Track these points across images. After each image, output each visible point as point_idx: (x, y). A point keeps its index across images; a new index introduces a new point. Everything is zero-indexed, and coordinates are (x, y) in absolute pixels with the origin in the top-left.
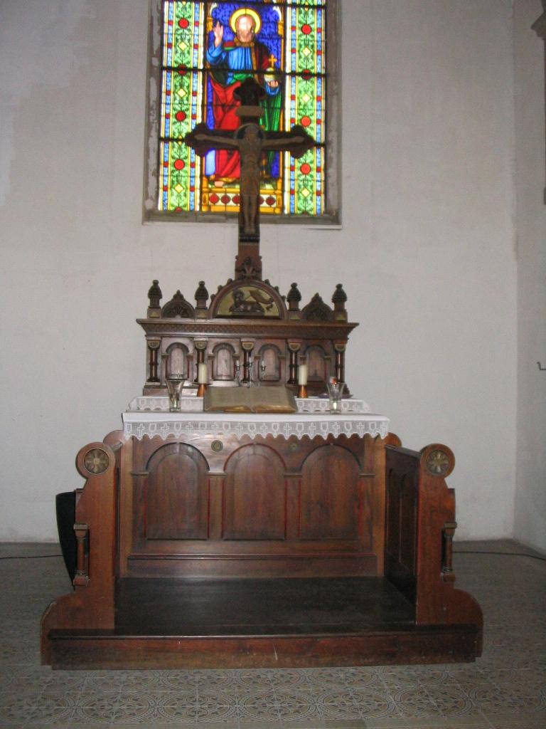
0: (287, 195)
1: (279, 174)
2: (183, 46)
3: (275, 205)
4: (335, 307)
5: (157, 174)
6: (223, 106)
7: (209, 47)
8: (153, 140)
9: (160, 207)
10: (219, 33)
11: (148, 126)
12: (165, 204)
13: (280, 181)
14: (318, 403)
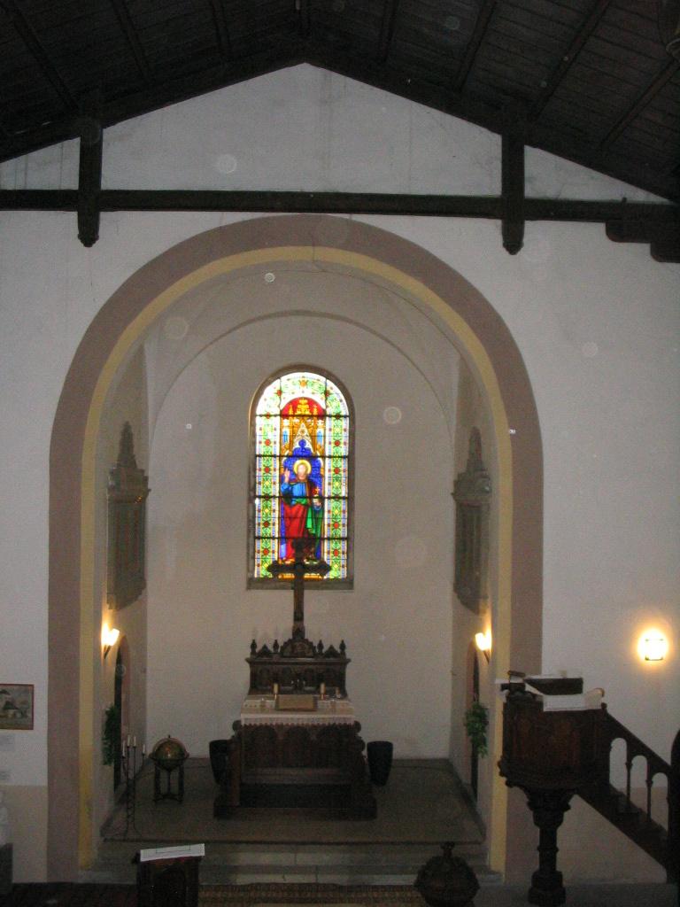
2: (267, 483)
5: (254, 558)
6: (290, 518)
8: (252, 539)
9: (256, 576)
10: (287, 474)
11: (249, 531)
12: (258, 574)
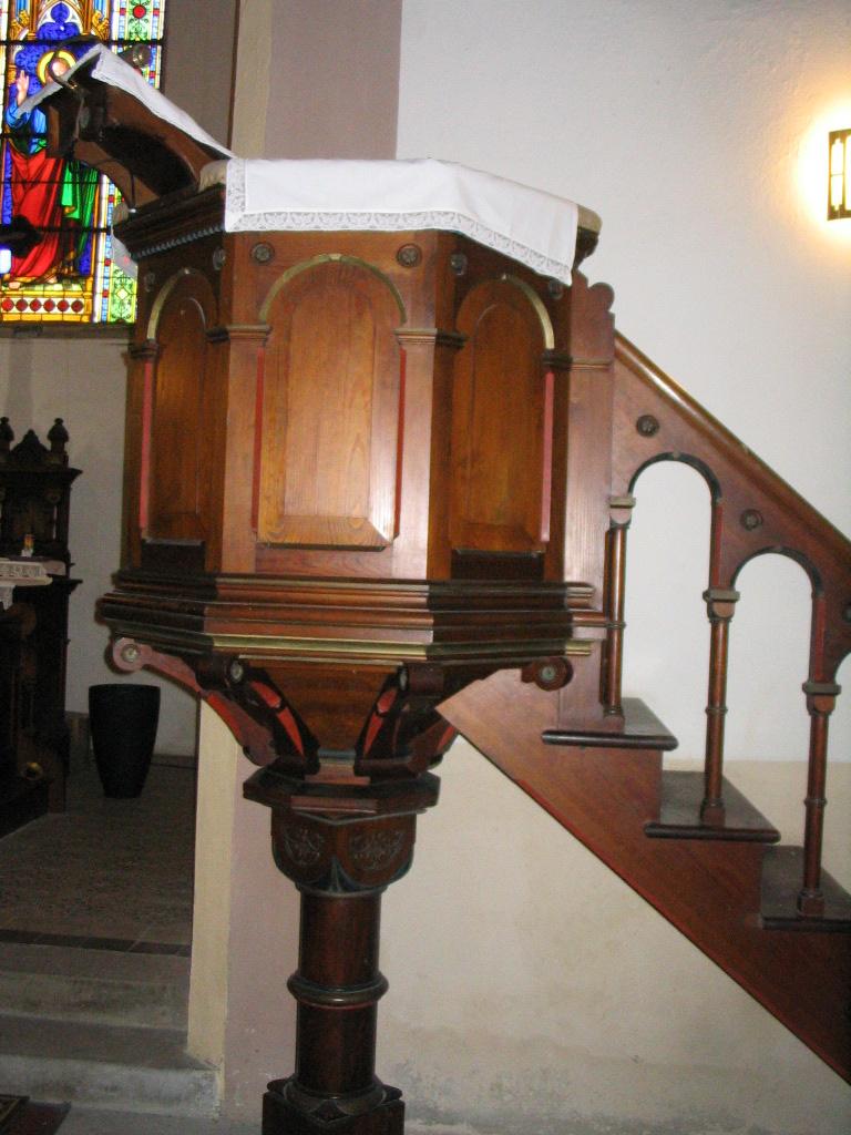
0: (99, 298)
1: (90, 271)
3: (82, 312)
4: (52, 447)
6: (24, 182)
7: (10, 104)
13: (91, 279)
14: (11, 567)
